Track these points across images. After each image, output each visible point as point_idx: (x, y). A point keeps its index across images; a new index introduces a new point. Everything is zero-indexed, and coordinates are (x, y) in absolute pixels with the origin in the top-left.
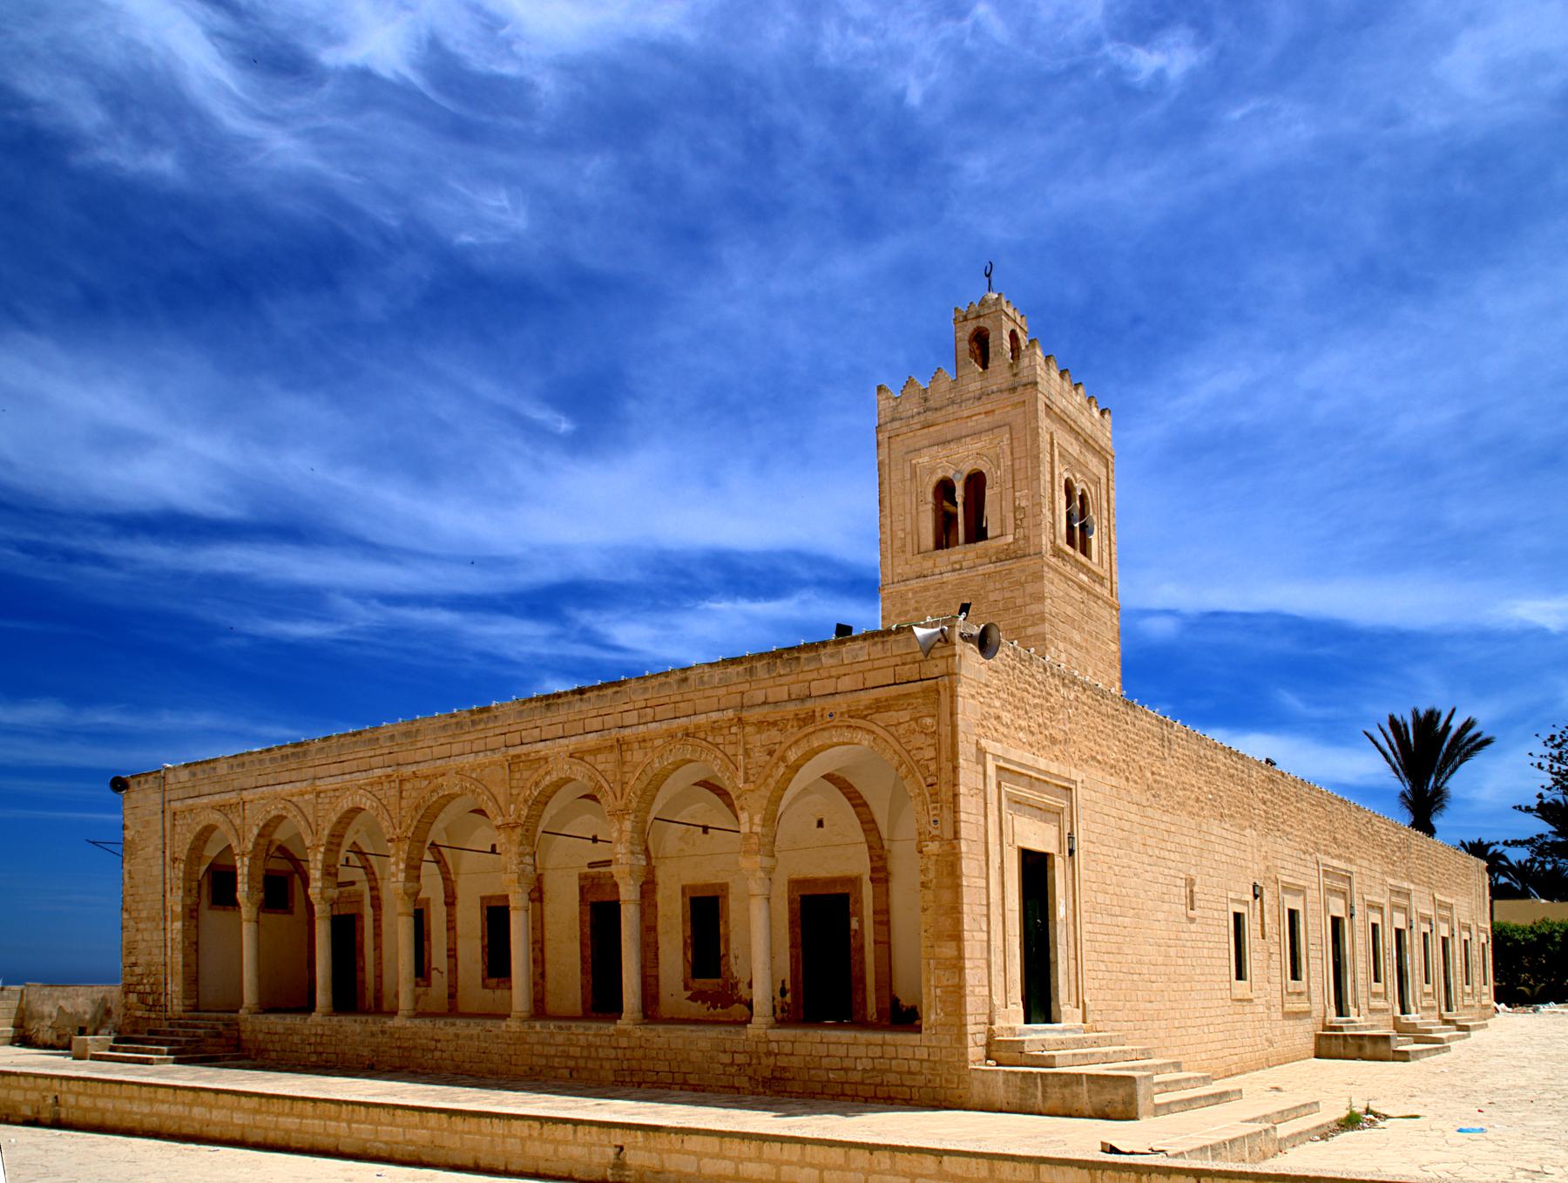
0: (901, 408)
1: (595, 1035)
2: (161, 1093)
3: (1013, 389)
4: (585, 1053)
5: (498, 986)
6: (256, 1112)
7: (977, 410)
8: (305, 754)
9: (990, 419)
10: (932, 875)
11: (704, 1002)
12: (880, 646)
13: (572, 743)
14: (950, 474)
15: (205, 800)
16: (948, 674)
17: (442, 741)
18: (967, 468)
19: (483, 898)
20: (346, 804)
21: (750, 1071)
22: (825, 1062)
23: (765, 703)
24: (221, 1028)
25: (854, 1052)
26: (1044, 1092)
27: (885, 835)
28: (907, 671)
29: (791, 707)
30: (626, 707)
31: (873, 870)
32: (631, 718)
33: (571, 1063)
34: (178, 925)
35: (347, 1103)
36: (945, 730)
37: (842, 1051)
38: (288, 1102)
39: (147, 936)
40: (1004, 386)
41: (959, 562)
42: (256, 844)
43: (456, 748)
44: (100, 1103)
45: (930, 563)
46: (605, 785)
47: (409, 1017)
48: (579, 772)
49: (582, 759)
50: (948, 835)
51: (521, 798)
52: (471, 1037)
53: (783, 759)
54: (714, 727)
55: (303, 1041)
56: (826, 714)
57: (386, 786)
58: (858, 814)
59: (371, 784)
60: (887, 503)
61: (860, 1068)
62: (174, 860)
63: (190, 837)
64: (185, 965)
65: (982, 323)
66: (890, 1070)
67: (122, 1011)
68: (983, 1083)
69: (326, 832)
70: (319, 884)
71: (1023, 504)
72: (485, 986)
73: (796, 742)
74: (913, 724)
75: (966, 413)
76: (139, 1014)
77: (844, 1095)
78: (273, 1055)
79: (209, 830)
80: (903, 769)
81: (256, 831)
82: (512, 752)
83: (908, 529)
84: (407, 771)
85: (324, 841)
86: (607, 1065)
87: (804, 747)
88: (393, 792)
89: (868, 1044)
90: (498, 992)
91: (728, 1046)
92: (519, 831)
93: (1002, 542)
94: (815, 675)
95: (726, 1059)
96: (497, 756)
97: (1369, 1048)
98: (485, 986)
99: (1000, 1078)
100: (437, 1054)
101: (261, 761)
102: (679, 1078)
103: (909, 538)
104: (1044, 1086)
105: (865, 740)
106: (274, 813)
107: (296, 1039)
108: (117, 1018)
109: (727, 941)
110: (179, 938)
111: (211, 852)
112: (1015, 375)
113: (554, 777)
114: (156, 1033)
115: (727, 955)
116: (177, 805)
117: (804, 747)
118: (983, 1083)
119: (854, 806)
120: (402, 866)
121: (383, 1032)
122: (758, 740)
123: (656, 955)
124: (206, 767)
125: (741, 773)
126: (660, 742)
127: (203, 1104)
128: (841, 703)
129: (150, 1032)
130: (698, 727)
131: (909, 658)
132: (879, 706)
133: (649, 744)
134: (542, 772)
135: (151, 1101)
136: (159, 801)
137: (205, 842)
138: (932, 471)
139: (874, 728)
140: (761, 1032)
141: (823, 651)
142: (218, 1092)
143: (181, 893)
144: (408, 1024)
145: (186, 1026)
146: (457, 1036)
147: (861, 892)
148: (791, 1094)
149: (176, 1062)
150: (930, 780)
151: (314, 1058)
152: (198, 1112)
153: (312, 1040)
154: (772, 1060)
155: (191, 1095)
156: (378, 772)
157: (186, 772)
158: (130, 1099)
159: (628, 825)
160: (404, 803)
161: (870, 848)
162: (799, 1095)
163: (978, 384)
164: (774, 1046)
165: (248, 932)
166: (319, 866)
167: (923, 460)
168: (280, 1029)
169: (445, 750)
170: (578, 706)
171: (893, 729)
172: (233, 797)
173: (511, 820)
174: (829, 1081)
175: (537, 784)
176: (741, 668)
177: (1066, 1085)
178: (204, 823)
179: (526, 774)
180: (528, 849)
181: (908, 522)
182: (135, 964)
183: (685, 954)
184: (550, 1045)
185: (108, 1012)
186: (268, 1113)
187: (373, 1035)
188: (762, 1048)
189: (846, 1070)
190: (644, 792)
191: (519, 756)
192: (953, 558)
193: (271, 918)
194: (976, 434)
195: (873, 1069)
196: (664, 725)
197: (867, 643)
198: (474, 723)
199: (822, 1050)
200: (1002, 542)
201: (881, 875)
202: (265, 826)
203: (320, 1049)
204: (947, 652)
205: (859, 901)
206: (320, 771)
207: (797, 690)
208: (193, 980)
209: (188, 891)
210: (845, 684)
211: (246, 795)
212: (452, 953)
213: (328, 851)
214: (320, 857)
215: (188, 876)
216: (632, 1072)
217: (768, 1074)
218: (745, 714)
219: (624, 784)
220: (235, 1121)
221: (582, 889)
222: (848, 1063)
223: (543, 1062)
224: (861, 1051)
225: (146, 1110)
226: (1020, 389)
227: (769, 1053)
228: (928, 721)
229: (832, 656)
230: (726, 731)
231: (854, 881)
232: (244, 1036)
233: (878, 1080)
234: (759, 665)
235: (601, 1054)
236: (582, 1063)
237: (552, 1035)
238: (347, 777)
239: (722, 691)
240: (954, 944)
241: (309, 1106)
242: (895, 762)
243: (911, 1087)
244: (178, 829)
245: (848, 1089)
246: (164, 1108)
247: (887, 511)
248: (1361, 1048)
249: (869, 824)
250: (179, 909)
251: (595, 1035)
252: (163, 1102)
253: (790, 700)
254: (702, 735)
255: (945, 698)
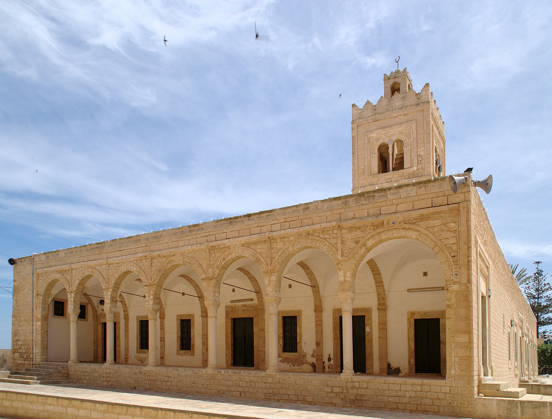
0: (363, 113)
1: (254, 377)
2: (49, 400)
3: (418, 105)
4: (248, 385)
5: (185, 354)
6: (105, 412)
7: (400, 114)
8: (103, 247)
9: (406, 117)
10: (453, 301)
11: (288, 363)
12: (423, 189)
13: (244, 240)
14: (386, 141)
15: (53, 268)
16: (465, 201)
17: (174, 240)
18: (395, 138)
19: (178, 316)
20: (123, 269)
21: (342, 396)
22: (387, 393)
23: (354, 218)
24: (60, 369)
25: (404, 388)
26: (522, 411)
27: (386, 288)
28: (438, 201)
29: (370, 220)
30: (274, 222)
31: (379, 305)
32: (277, 227)
33: (241, 389)
34: (39, 323)
35: (162, 409)
36: (463, 229)
37: (397, 387)
38: (125, 408)
39: (24, 328)
40: (413, 103)
41: (391, 179)
42: (78, 288)
43: (181, 243)
44: (15, 404)
45: (376, 179)
46: (262, 259)
47: (154, 366)
48: (247, 253)
49: (249, 247)
50: (465, 281)
51: (215, 266)
52: (187, 376)
53: (364, 245)
54: (324, 231)
55: (99, 376)
56: (391, 222)
57: (144, 261)
58: (375, 279)
59: (136, 261)
60: (356, 154)
61: (407, 395)
62: (38, 295)
63: (45, 285)
64: (42, 341)
65: (397, 80)
66: (426, 398)
67: (12, 360)
68: (484, 405)
69: (113, 282)
70: (109, 306)
71: (422, 153)
72: (178, 354)
73: (372, 237)
74: (443, 226)
75: (395, 115)
76: (20, 362)
77: (398, 409)
78: (85, 382)
79: (54, 282)
80: (437, 249)
81: (78, 282)
82: (211, 244)
83: (366, 164)
84: (155, 254)
85: (112, 286)
86: (260, 391)
87: (377, 239)
88: (147, 264)
89: (413, 385)
90: (185, 357)
91: (329, 383)
92: (214, 281)
93: (411, 170)
94: (384, 204)
95: (329, 390)
96: (203, 247)
97: (543, 390)
98: (178, 354)
99: (495, 403)
100: (169, 383)
101: (81, 251)
102: (301, 398)
103: (366, 169)
104: (522, 407)
105: (414, 235)
106: (86, 274)
107: (97, 375)
108: (9, 364)
109: (301, 336)
110: (40, 329)
111: (55, 292)
112: (419, 98)
113: (234, 256)
114: (29, 370)
115: (300, 342)
116: (40, 271)
117: (377, 239)
118: (484, 405)
119: (374, 275)
120: (152, 297)
121: (141, 373)
122: (349, 237)
123: (264, 342)
124: (54, 254)
125: (340, 252)
126: (293, 238)
127: (73, 407)
128: (400, 217)
129: (26, 370)
130: (315, 231)
131: (441, 194)
132: (422, 218)
133: (286, 239)
134: (227, 253)
135: (44, 404)
136: (31, 269)
137: (52, 287)
138: (378, 140)
139: (420, 229)
140: (349, 377)
141: (388, 192)
142: (83, 401)
143: (41, 309)
144: (154, 369)
145: (43, 367)
146: (179, 375)
147: (371, 315)
148: (366, 408)
149: (42, 383)
150: (453, 254)
151: (105, 383)
152: (70, 410)
153: (105, 375)
154: (355, 391)
155: (67, 402)
156: (140, 255)
157: (44, 256)
158: (32, 403)
159: (274, 278)
160: (153, 269)
161: (378, 294)
162: (371, 408)
163: (401, 103)
164: (357, 385)
165: (73, 327)
166: (109, 297)
167: (374, 135)
168: (88, 370)
169: (175, 244)
170: (247, 222)
171: (431, 229)
172: (67, 267)
173: (209, 276)
174: (389, 402)
175: (224, 259)
176: (340, 202)
177: (536, 407)
178: (53, 279)
179: (218, 255)
180: (217, 290)
181: (366, 162)
182: (18, 340)
183: (279, 341)
184: (229, 380)
185: (5, 361)
186: (113, 413)
187: (135, 373)
188: (350, 385)
189: (399, 397)
190: (283, 262)
191: (215, 246)
192: (387, 177)
193: (82, 322)
194: (400, 124)
195: (416, 396)
196: (296, 230)
197: (415, 187)
198: (190, 231)
199: (385, 387)
200: (411, 170)
201: (383, 307)
202: (83, 280)
203: (108, 379)
204: (465, 190)
205: (370, 319)
206: (110, 255)
207: (372, 211)
208: (45, 348)
209: (44, 309)
210: (401, 208)
211: (73, 266)
212: (162, 340)
213: (113, 290)
214: (109, 293)
215: (44, 302)
216: (274, 394)
217: (353, 397)
218: (343, 224)
219: (272, 258)
220: (93, 416)
221: (227, 312)
222: (400, 393)
223: (225, 388)
224: (409, 388)
225: (41, 408)
226: (421, 104)
227: (353, 388)
228: (452, 225)
229: (394, 194)
230: (330, 232)
231: (369, 310)
232: (70, 373)
233: (419, 402)
234: (350, 200)
235: (257, 385)
236: (246, 389)
237: (230, 375)
238: (124, 257)
239: (329, 213)
240: (467, 336)
241: (138, 411)
242: (432, 245)
243: (439, 406)
244: (40, 281)
245: (400, 406)
246: (51, 408)
247: (356, 157)
248: (539, 390)
249: (379, 283)
250: (40, 316)
251: (254, 377)
252: (50, 405)
253: (368, 216)
254: (317, 234)
255: (463, 213)
